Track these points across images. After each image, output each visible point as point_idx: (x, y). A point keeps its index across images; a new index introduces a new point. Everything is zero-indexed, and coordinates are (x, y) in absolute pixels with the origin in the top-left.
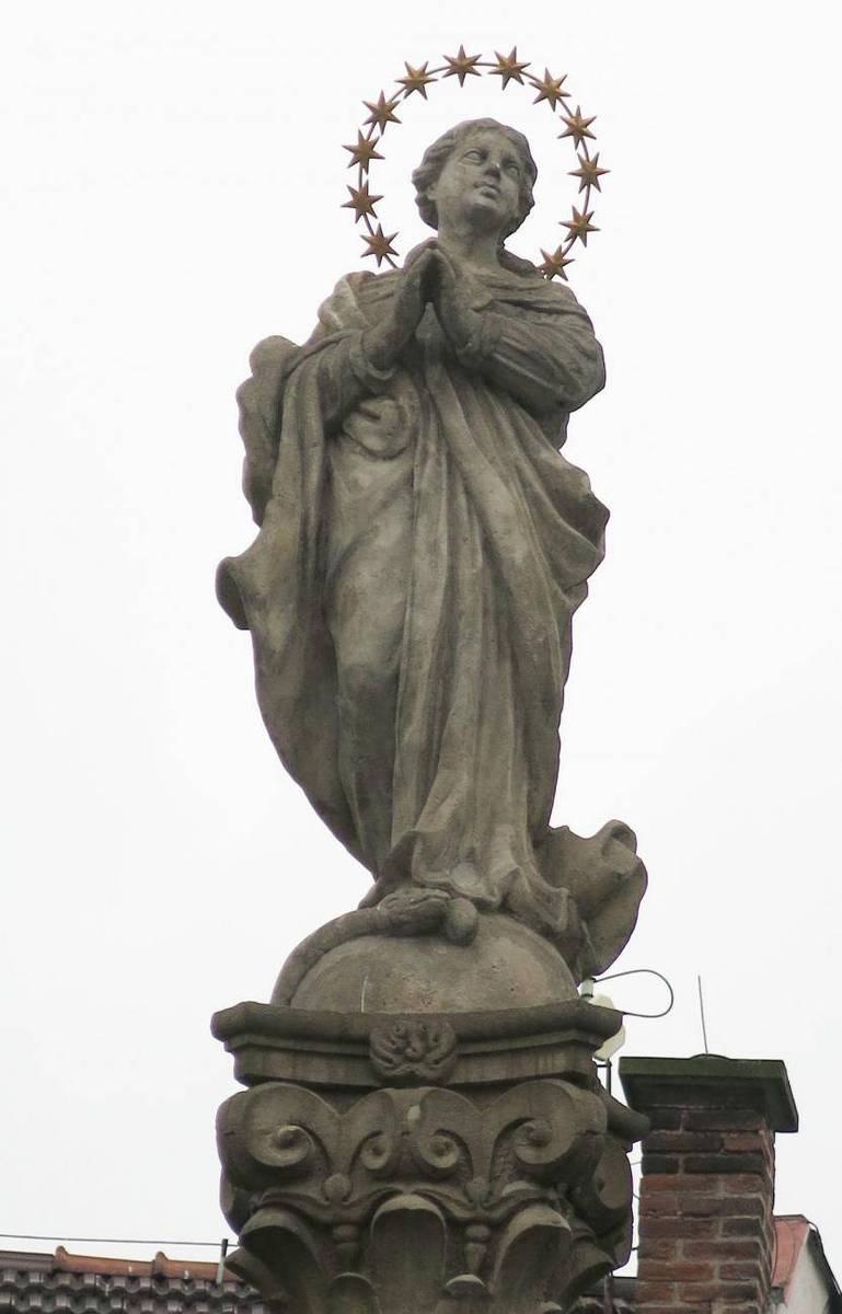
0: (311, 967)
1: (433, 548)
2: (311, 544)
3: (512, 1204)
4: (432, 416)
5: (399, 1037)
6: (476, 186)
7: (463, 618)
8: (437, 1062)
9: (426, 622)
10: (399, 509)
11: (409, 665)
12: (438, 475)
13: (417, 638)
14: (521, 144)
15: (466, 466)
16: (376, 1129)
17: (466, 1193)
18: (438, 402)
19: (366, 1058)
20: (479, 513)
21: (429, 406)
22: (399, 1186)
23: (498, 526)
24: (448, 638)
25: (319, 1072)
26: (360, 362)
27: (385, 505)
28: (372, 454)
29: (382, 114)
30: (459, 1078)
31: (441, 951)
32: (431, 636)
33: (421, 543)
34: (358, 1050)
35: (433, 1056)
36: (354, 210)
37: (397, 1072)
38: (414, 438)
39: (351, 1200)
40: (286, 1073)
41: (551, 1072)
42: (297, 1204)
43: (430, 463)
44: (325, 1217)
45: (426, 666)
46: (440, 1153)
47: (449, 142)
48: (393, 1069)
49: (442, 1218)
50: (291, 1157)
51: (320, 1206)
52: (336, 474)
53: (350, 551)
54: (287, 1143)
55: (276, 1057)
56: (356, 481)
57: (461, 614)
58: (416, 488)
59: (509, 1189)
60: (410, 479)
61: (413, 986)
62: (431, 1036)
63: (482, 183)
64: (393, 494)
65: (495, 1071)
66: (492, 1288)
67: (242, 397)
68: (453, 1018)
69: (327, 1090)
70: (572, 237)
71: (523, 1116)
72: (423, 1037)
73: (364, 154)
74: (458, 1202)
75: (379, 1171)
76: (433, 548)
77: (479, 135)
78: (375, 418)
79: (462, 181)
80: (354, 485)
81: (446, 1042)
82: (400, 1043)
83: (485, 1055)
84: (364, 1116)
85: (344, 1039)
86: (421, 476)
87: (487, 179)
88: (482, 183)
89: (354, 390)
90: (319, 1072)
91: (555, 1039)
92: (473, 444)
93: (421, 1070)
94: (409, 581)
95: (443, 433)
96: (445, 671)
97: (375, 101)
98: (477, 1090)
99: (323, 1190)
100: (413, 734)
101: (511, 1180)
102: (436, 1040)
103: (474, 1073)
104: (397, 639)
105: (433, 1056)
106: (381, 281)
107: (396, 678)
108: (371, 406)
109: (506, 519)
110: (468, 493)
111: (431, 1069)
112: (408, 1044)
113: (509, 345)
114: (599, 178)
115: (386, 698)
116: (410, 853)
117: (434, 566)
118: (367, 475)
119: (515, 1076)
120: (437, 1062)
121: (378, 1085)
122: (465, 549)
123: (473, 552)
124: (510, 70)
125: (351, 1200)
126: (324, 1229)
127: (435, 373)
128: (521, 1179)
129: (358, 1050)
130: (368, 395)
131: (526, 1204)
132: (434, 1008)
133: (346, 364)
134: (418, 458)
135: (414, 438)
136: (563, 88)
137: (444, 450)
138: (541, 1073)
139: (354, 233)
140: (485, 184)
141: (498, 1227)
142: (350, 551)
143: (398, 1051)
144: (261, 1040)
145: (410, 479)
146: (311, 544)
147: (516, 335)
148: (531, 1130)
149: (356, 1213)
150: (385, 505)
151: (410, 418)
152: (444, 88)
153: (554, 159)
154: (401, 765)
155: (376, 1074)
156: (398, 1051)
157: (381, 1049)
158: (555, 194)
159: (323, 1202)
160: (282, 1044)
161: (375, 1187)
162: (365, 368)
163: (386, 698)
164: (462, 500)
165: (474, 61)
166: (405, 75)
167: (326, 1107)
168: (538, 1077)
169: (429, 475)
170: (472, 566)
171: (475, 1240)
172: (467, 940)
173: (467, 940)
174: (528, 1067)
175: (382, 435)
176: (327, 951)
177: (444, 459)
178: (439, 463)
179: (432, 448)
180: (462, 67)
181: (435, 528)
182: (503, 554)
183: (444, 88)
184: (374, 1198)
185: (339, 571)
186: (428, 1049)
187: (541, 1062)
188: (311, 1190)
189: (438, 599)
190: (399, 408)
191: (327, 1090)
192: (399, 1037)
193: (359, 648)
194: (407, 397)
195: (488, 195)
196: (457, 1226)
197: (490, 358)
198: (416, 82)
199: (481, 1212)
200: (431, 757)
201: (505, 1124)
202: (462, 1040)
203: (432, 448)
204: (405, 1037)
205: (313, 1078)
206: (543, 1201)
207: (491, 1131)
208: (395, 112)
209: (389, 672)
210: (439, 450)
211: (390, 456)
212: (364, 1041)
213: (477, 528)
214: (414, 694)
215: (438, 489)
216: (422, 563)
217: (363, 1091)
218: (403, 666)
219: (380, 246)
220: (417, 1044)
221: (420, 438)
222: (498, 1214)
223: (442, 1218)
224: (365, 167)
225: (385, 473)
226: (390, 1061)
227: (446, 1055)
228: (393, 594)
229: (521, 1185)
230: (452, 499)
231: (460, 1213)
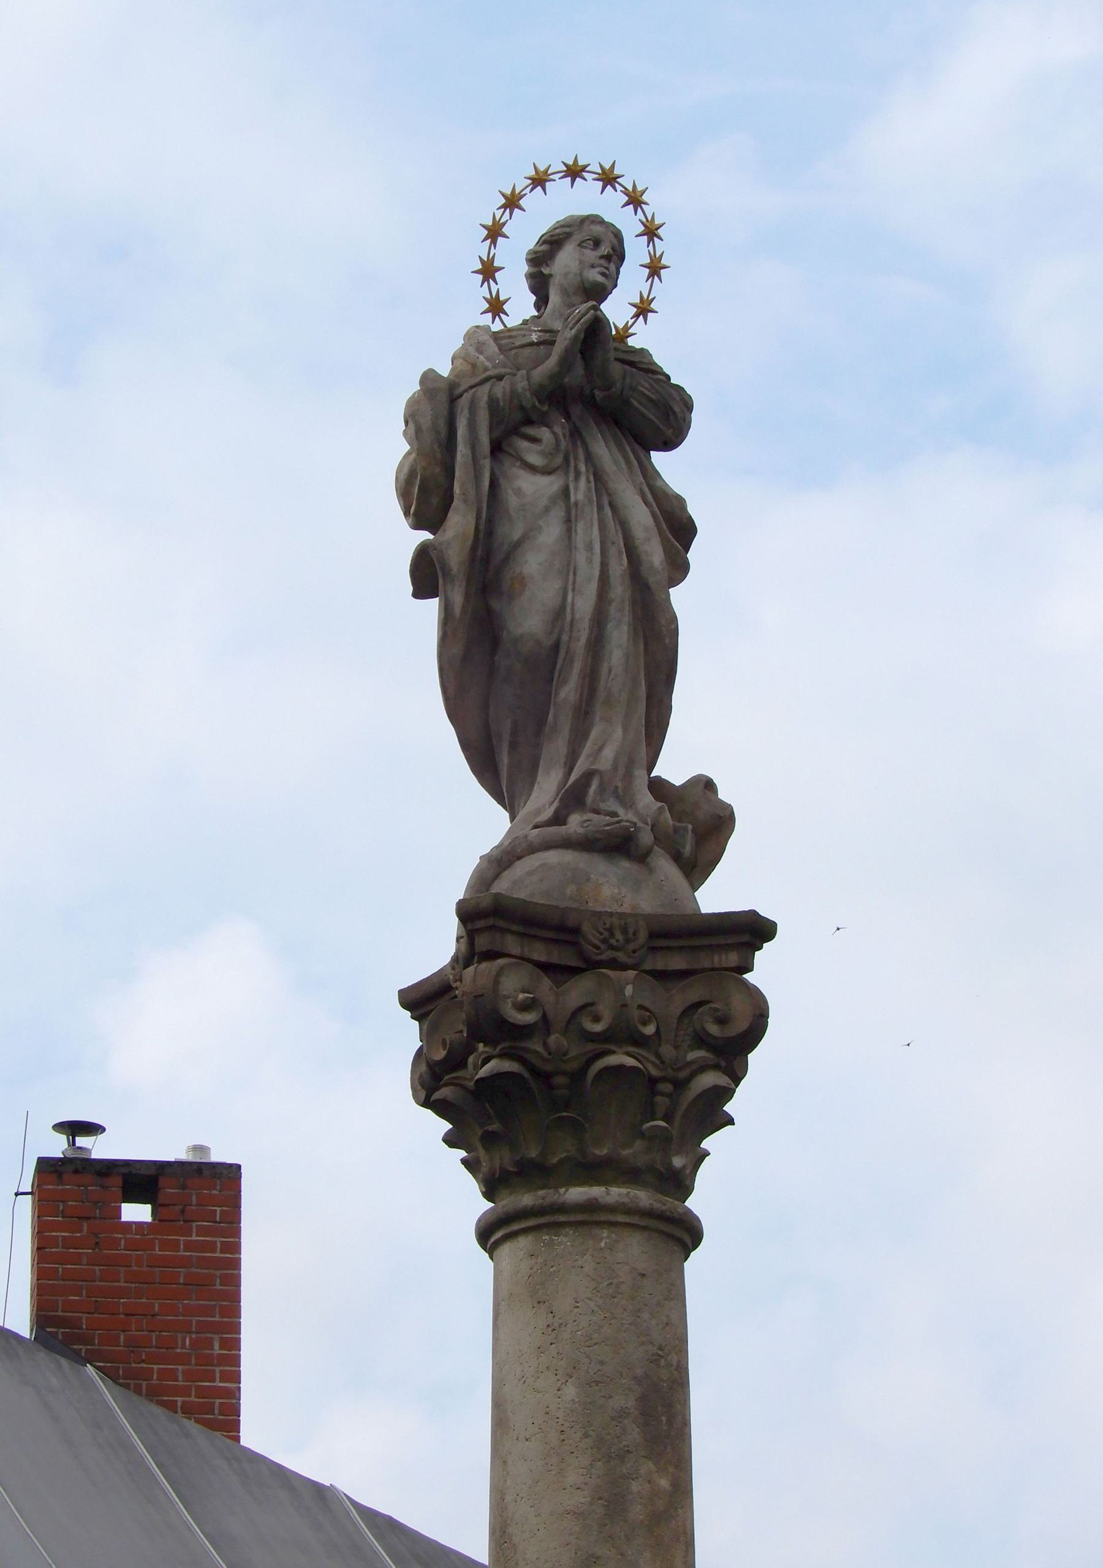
0: (504, 870)
1: (589, 547)
2: (481, 536)
3: (694, 1067)
4: (579, 443)
5: (605, 929)
6: (593, 266)
7: (614, 605)
8: (634, 952)
9: (584, 605)
10: (558, 513)
11: (570, 637)
12: (589, 489)
13: (577, 616)
14: (618, 236)
15: (611, 485)
16: (589, 1000)
17: (658, 1056)
18: (584, 434)
19: (576, 944)
20: (624, 525)
21: (576, 434)
22: (613, 1048)
23: (639, 533)
24: (599, 620)
25: (539, 953)
26: (528, 394)
27: (547, 510)
28: (532, 469)
29: (512, 202)
30: (648, 966)
31: (625, 865)
32: (588, 617)
33: (580, 538)
34: (570, 938)
35: (631, 946)
36: (647, 271)
37: (603, 957)
38: (566, 460)
39: (569, 1056)
40: (516, 950)
41: (725, 965)
42: (527, 1056)
43: (583, 479)
44: (548, 1068)
45: (583, 640)
46: (645, 1023)
47: (567, 230)
48: (600, 954)
49: (526, 1075)
50: (529, 1018)
51: (543, 1059)
52: (503, 482)
53: (518, 544)
54: (524, 1007)
55: (509, 938)
56: (520, 488)
57: (610, 603)
58: (573, 499)
59: (692, 1056)
60: (565, 492)
61: (607, 891)
62: (631, 931)
63: (579, 261)
64: (553, 500)
65: (677, 963)
66: (674, 1132)
67: (411, 417)
68: (647, 917)
69: (545, 968)
70: (636, 316)
71: (703, 999)
72: (624, 931)
73: (494, 233)
74: (654, 1064)
75: (598, 1034)
76: (589, 547)
77: (593, 227)
78: (534, 440)
79: (581, 262)
80: (519, 492)
81: (643, 935)
82: (606, 934)
83: (669, 948)
84: (577, 991)
85: (561, 928)
86: (576, 489)
87: (603, 262)
88: (579, 261)
89: (518, 416)
90: (539, 953)
91: (731, 940)
92: (615, 468)
93: (621, 957)
94: (568, 570)
95: (589, 457)
96: (597, 643)
97: (508, 192)
98: (661, 976)
99: (545, 1044)
100: (568, 692)
101: (692, 1048)
102: (634, 934)
103: (661, 963)
104: (559, 613)
105: (631, 946)
106: (514, 333)
107: (556, 646)
108: (531, 431)
109: (646, 529)
110: (612, 506)
111: (629, 957)
112: (612, 935)
113: (644, 394)
114: (662, 271)
115: (547, 662)
116: (587, 785)
117: (590, 561)
118: (529, 488)
119: (696, 966)
120: (634, 952)
121: (583, 966)
122: (612, 551)
123: (620, 553)
124: (608, 179)
125: (569, 1056)
126: (543, 1077)
127: (576, 410)
128: (699, 1048)
129: (570, 938)
130: (529, 422)
131: (703, 1068)
132: (626, 908)
133: (513, 393)
134: (571, 477)
135: (566, 460)
136: (645, 198)
137: (591, 470)
138: (717, 966)
139: (477, 293)
140: (601, 266)
141: (679, 1085)
142: (518, 544)
143: (604, 941)
144: (501, 923)
145: (565, 492)
146: (481, 536)
147: (647, 385)
148: (716, 1010)
149: (573, 1066)
150: (547, 510)
151: (563, 444)
152: (559, 186)
153: (636, 251)
154: (555, 716)
155: (581, 955)
156: (604, 941)
157: (590, 937)
158: (631, 280)
159: (545, 1054)
160: (515, 928)
161: (591, 1046)
162: (529, 400)
163: (547, 662)
164: (608, 511)
165: (584, 169)
166: (532, 173)
167: (546, 983)
168: (713, 969)
169: (581, 491)
170: (619, 567)
171: (662, 1094)
172: (642, 858)
173: (642, 858)
174: (705, 961)
175: (542, 453)
176: (519, 858)
177: (592, 478)
178: (588, 481)
179: (582, 468)
180: (574, 172)
181: (587, 532)
182: (643, 557)
183: (559, 186)
184: (590, 1055)
185: (508, 557)
186: (627, 941)
187: (716, 958)
188: (535, 1045)
189: (592, 589)
190: (554, 434)
191: (545, 968)
192: (605, 929)
193: (527, 621)
194: (560, 426)
195: (603, 274)
196: (653, 1081)
197: (627, 402)
198: (539, 181)
199: (670, 1073)
200: (584, 714)
201: (687, 1004)
202: (653, 935)
203: (582, 468)
204: (611, 931)
205: (536, 957)
206: (716, 1067)
207: (676, 1008)
208: (522, 202)
209: (548, 643)
210: (587, 471)
211: (547, 471)
212: (576, 931)
213: (620, 535)
214: (572, 661)
215: (590, 501)
216: (581, 557)
217: (573, 971)
218: (565, 638)
219: (496, 307)
220: (619, 936)
221: (572, 459)
222: (682, 1075)
223: (526, 1075)
224: (494, 243)
225: (549, 485)
226: (597, 948)
227: (643, 946)
228: (552, 580)
229: (701, 1053)
230: (600, 508)
231: (654, 1072)
